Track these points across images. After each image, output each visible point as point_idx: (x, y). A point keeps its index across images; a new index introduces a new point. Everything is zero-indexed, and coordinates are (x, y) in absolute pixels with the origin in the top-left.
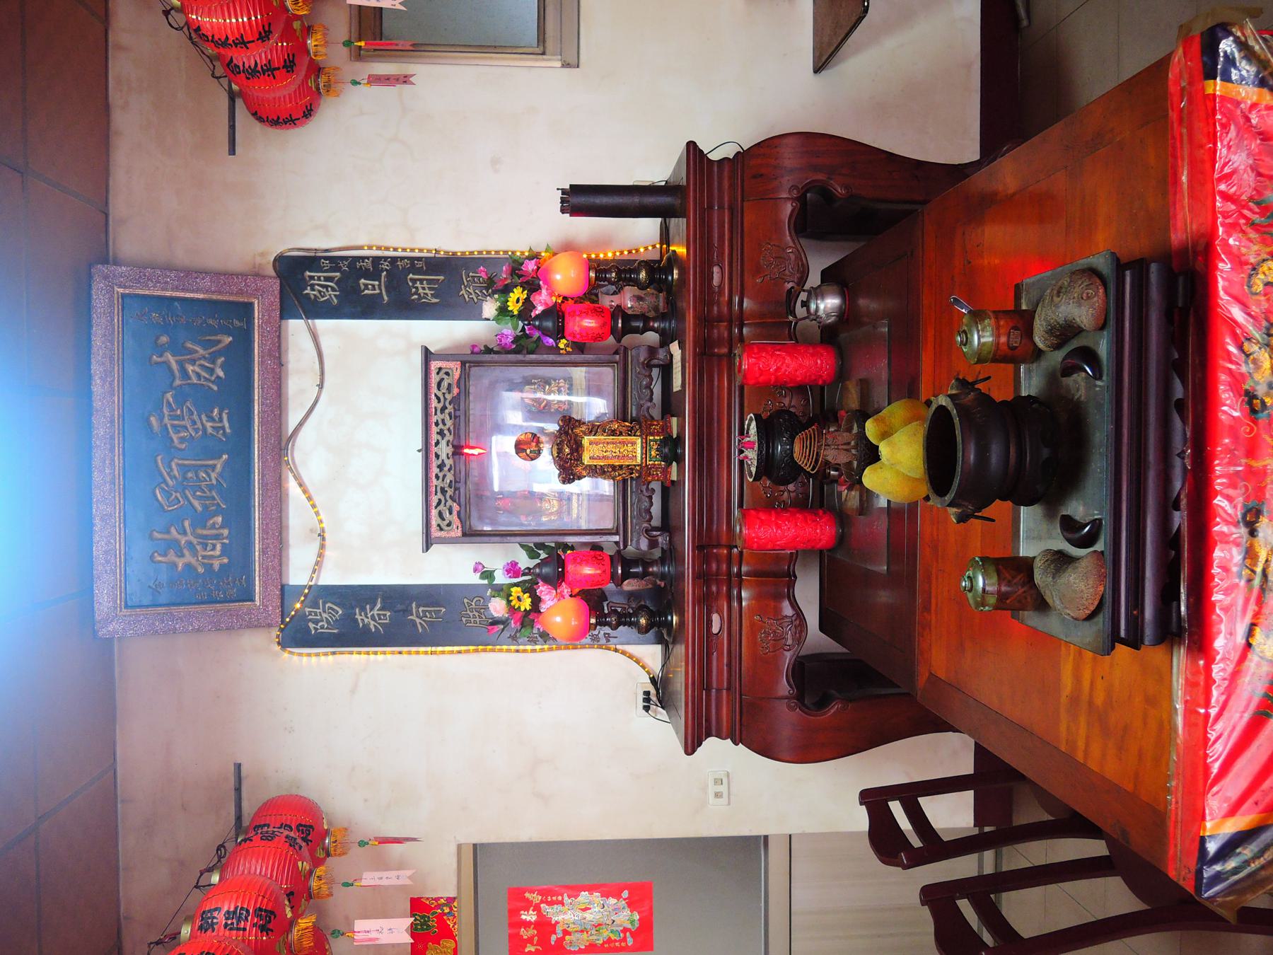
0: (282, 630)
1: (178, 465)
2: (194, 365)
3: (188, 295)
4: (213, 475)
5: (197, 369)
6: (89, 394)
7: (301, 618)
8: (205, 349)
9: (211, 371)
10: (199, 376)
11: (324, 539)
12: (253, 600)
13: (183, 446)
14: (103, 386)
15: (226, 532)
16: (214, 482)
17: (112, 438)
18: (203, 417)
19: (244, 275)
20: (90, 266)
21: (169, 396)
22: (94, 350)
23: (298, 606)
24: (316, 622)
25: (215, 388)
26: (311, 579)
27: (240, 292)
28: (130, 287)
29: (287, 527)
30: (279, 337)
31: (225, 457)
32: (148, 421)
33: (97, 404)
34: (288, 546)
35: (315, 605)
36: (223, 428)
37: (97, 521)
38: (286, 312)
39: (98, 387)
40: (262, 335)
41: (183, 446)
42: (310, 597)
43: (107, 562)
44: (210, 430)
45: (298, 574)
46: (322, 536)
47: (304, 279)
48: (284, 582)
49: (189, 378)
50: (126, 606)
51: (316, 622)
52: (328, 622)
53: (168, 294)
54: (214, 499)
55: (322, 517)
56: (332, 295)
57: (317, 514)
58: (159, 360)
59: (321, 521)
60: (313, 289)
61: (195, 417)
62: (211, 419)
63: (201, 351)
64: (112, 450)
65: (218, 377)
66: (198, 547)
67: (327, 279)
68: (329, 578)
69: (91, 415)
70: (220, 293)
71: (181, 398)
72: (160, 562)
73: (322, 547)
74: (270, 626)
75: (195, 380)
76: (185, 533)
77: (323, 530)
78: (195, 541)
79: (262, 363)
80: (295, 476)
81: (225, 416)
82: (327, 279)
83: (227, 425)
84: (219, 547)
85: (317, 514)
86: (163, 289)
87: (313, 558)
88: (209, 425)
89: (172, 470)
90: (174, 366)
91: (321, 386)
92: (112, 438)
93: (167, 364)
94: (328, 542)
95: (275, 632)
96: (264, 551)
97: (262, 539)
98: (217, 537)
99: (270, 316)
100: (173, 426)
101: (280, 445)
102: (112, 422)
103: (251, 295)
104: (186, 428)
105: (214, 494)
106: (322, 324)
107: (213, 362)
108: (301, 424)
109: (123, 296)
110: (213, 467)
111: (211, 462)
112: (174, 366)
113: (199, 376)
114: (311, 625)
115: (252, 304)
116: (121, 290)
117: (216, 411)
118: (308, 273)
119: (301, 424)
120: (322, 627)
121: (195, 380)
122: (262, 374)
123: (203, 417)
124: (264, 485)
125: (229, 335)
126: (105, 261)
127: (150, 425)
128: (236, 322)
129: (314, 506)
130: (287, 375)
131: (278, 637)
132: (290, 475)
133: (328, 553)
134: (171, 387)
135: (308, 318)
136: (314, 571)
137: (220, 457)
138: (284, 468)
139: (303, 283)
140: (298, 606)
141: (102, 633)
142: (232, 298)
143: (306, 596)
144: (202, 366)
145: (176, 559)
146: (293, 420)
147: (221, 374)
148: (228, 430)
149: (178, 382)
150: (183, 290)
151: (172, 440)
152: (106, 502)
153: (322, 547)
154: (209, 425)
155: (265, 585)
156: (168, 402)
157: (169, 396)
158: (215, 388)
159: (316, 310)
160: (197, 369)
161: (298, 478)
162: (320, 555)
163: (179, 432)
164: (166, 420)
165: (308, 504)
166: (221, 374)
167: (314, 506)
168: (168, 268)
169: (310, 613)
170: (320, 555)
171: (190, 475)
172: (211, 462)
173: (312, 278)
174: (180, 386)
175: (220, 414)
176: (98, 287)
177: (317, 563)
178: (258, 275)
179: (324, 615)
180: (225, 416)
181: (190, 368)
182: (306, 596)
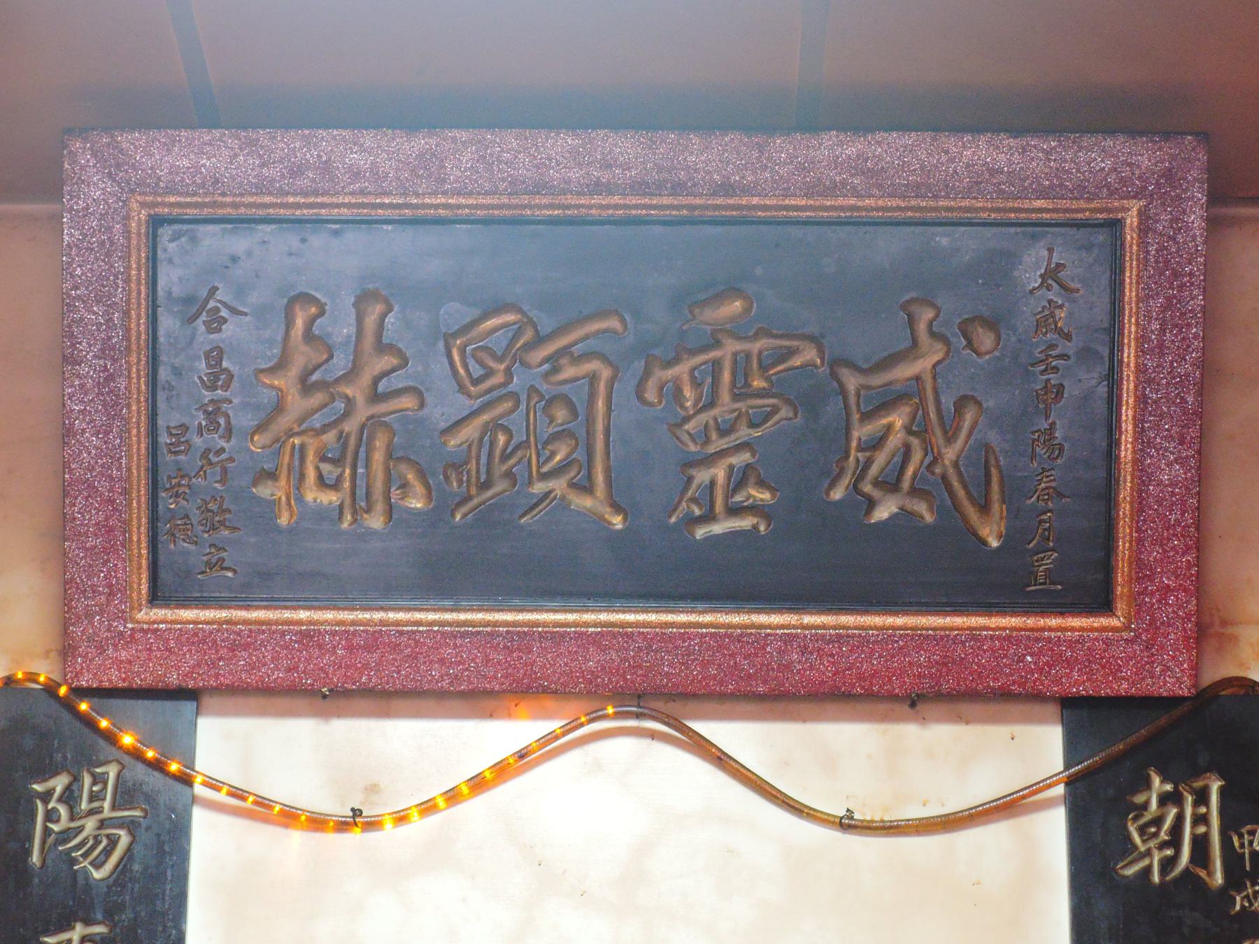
0: (50, 690)
1: (593, 378)
2: (909, 430)
3: (1127, 413)
4: (558, 486)
5: (895, 441)
6: (812, 126)
7: (89, 747)
8: (956, 464)
9: (890, 484)
10: (877, 443)
11: (343, 826)
12: (155, 598)
13: (651, 396)
14: (835, 163)
15: (376, 522)
16: (539, 488)
17: (678, 188)
18: (744, 458)
19: (1199, 584)
20: (1203, 136)
21: (809, 354)
22: (951, 143)
23: (127, 740)
24: (69, 797)
25: (837, 494)
26: (212, 784)
27: (1141, 570)
28: (1143, 245)
29: (386, 714)
30: (1005, 695)
31: (617, 522)
32: (733, 291)
33: (782, 148)
34: (325, 714)
35: (126, 795)
36: (709, 517)
37: (422, 142)
38: (1083, 715)
39: (833, 150)
40: (1011, 638)
41: (651, 396)
42: (154, 780)
43: (296, 171)
44: (702, 476)
45: (225, 744)
46: (355, 821)
47: (1197, 773)
48: (207, 701)
49: (866, 417)
50: (156, 222)
51: (69, 797)
52: (65, 836)
53: (1129, 355)
54: (486, 485)
55: (419, 826)
56: (1147, 860)
57: (428, 808)
58: (922, 327)
59: (401, 818)
60: (1164, 800)
61: (744, 433)
62: (740, 480)
63: (950, 454)
64: (640, 187)
65: (871, 504)
66: (330, 437)
67: (1201, 844)
68: (212, 841)
69: (747, 129)
70: (1140, 506)
71: (808, 397)
72: (289, 324)
73: (317, 823)
74: (67, 651)
75: (862, 432)
76: (376, 397)
77: (372, 825)
78: (350, 426)
79: (919, 639)
80: (552, 737)
81: (745, 523)
82: (1201, 844)
83: (718, 528)
84: (329, 498)
85: (428, 808)
86: (1142, 339)
87: (281, 791)
88: (719, 473)
89: (577, 360)
90: (904, 372)
91: (847, 824)
92: (678, 188)
93: (912, 350)
94: (332, 838)
95: (45, 671)
96: (309, 636)
97: (347, 635)
98: (359, 504)
99: (1070, 663)
100: (716, 365)
101: (659, 694)
102: (727, 189)
103: (1138, 609)
104: (711, 404)
105: (497, 488)
106: (1051, 830)
107: (914, 492)
108: (722, 760)
109: (1115, 225)
110: (586, 487)
111: (600, 478)
112: (904, 372)
113: (877, 443)
114: (59, 783)
115: (1105, 605)
116: (1131, 219)
117: (765, 496)
118: (1215, 787)
119: (722, 760)
120: (51, 816)
121: (862, 432)
122: (888, 635)
123: (744, 458)
124: (523, 638)
125: (1009, 540)
126: (1217, 196)
127: (720, 298)
128: (1049, 561)
129: (453, 796)
130: (885, 718)
131: (32, 677)
132: (554, 725)
133: (296, 839)
134: (835, 364)
135: (1070, 782)
136: (238, 794)
137: (617, 508)
138: (574, 708)
139: (1183, 771)
140: (127, 740)
141: (82, 155)
142: (1123, 547)
143: (158, 766)
144: (907, 451)
145: (294, 371)
146: (724, 733)
147: (882, 513)
148: (700, 532)
149: (852, 382)
150: (1142, 399)
151: (669, 364)
152: (477, 165)
153: (317, 823)
154: (719, 473)
155: (197, 638)
156: (792, 352)
157: (809, 354)
158: (837, 494)
159: (1097, 808)
160: (895, 441)
161: (524, 759)
162: (289, 817)
163: (697, 384)
164: (732, 346)
165: (434, 791)
166: (882, 513)
167: (453, 796)
168: (1209, 374)
169: (99, 779)
170: (289, 817)
171: (561, 414)
172: (600, 478)
173: (1202, 797)
174: (843, 392)
175: (754, 509)
176: (1146, 157)
177: (263, 803)
178: (1207, 630)
179: (90, 824)
180: (745, 523)
181: (898, 419)
182: (158, 766)
